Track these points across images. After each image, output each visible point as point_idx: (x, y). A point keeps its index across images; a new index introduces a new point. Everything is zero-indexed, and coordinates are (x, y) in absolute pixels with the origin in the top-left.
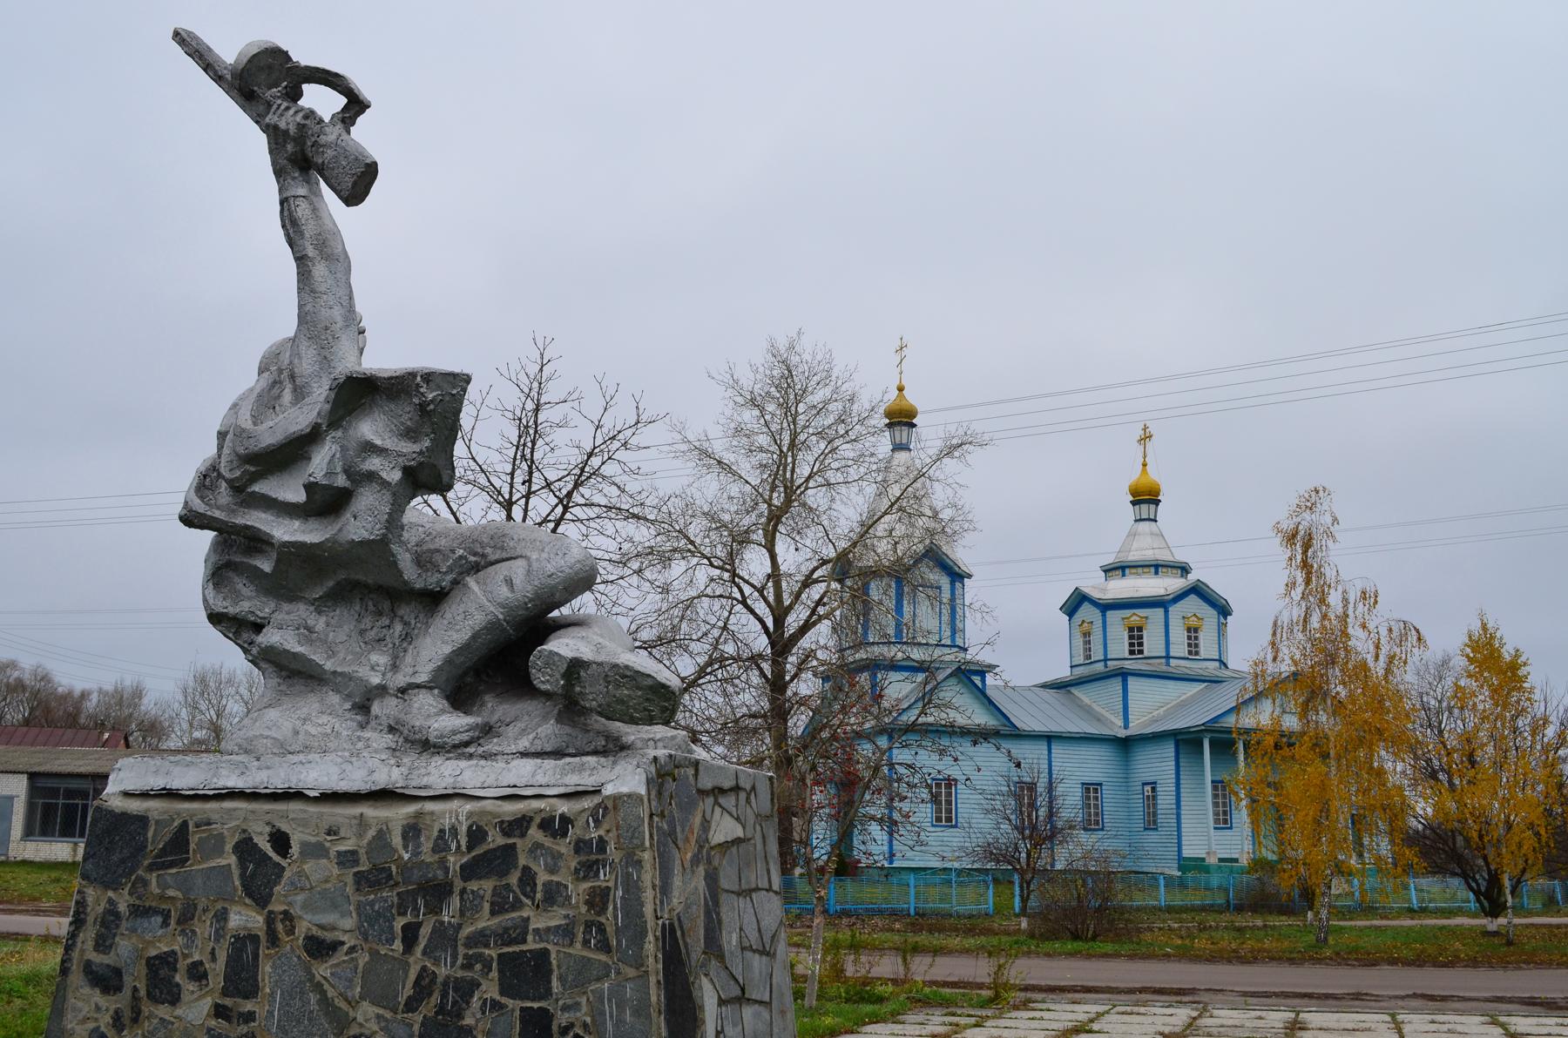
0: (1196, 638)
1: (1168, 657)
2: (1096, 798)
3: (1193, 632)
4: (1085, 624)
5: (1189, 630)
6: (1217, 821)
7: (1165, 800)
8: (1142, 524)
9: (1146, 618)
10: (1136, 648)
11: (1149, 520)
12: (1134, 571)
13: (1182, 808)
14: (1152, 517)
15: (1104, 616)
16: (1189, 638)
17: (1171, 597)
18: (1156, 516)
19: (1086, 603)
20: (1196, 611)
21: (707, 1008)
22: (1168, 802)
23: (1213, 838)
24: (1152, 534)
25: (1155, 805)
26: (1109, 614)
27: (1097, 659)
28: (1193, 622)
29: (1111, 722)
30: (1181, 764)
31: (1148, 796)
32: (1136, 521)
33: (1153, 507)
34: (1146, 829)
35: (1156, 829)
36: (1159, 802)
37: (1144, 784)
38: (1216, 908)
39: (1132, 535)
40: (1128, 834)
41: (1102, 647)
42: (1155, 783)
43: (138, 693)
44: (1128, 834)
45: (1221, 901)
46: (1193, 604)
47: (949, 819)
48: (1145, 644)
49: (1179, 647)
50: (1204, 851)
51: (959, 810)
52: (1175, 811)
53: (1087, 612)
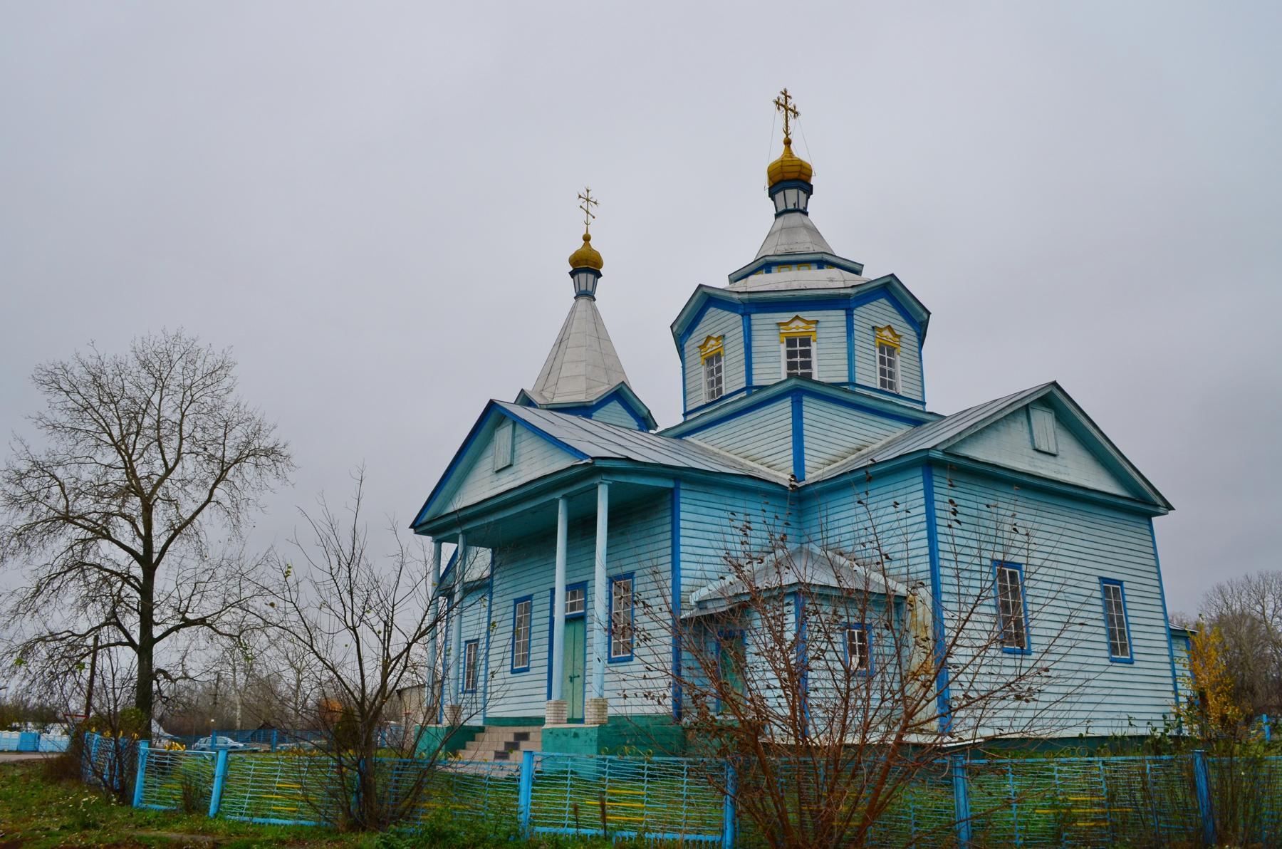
0: (891, 363)
4: (712, 342)
16: (882, 361)
18: (805, 208)
21: (769, 275)
32: (778, 215)
43: (218, 371)
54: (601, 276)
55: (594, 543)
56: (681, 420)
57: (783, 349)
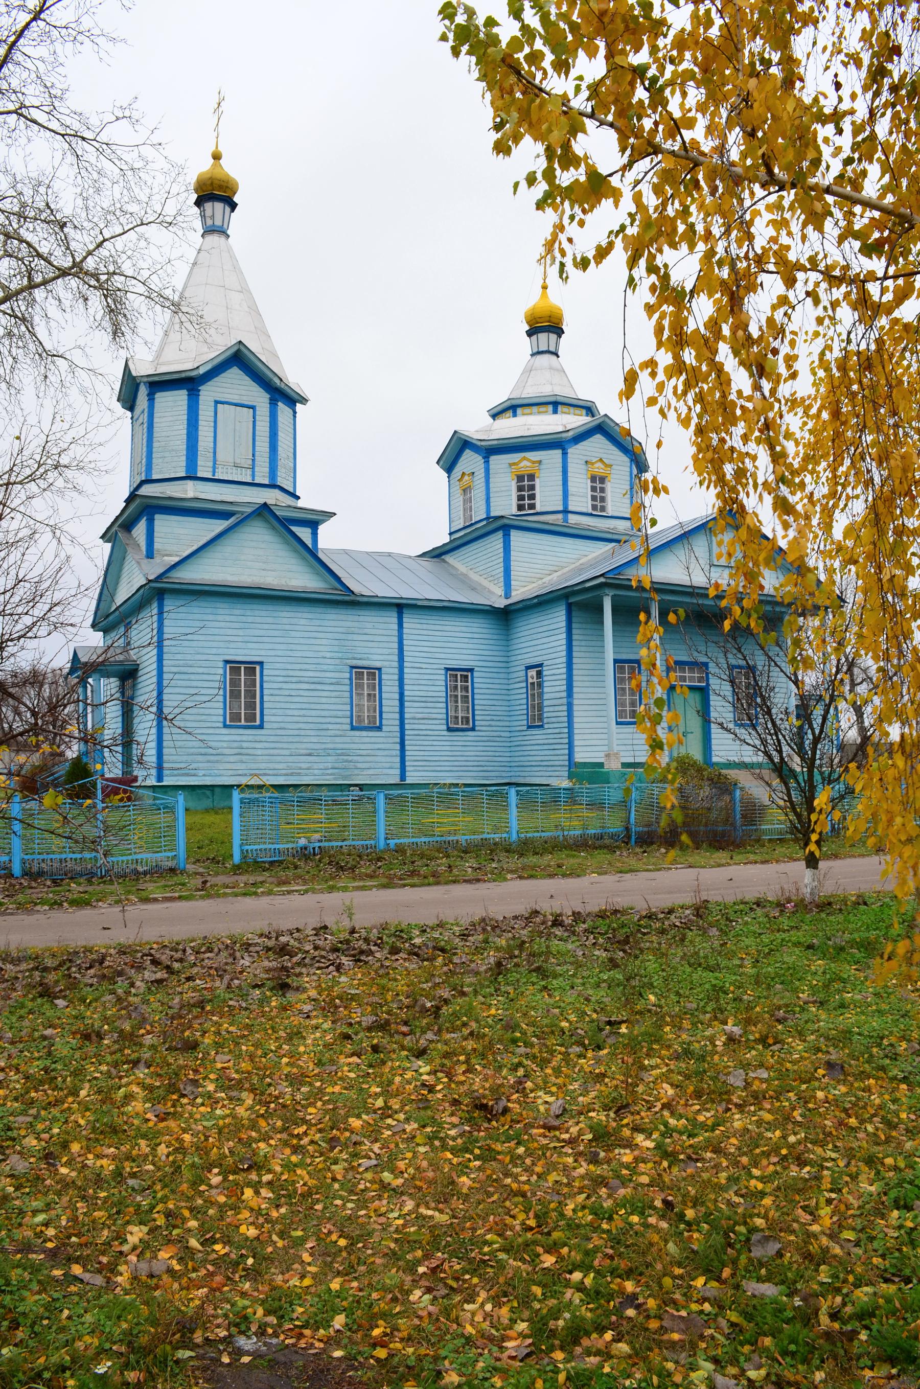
0: (602, 490)
1: (566, 511)
2: (466, 689)
3: (598, 482)
4: (466, 478)
5: (593, 479)
6: (620, 714)
7: (554, 687)
8: (539, 357)
9: (540, 462)
10: (527, 502)
11: (548, 352)
12: (527, 410)
13: (575, 696)
14: (552, 349)
15: (487, 462)
16: (593, 489)
17: (570, 434)
19: (467, 451)
20: (603, 456)
22: (557, 689)
23: (615, 736)
24: (551, 368)
25: (541, 695)
26: (494, 459)
27: (478, 519)
28: (599, 469)
29: (489, 591)
30: (574, 637)
31: (533, 684)
33: (553, 337)
34: (529, 727)
35: (542, 726)
36: (546, 690)
37: (528, 668)
38: (607, 841)
39: (529, 371)
40: (508, 734)
41: (484, 502)
42: (541, 665)
44: (508, 734)
45: (615, 826)
46: (598, 445)
47: (251, 718)
48: (538, 497)
49: (581, 500)
50: (602, 754)
51: (266, 705)
52: (565, 701)
53: (470, 461)
54: (584, 270)
55: (602, 623)
56: (447, 539)
57: (514, 485)
